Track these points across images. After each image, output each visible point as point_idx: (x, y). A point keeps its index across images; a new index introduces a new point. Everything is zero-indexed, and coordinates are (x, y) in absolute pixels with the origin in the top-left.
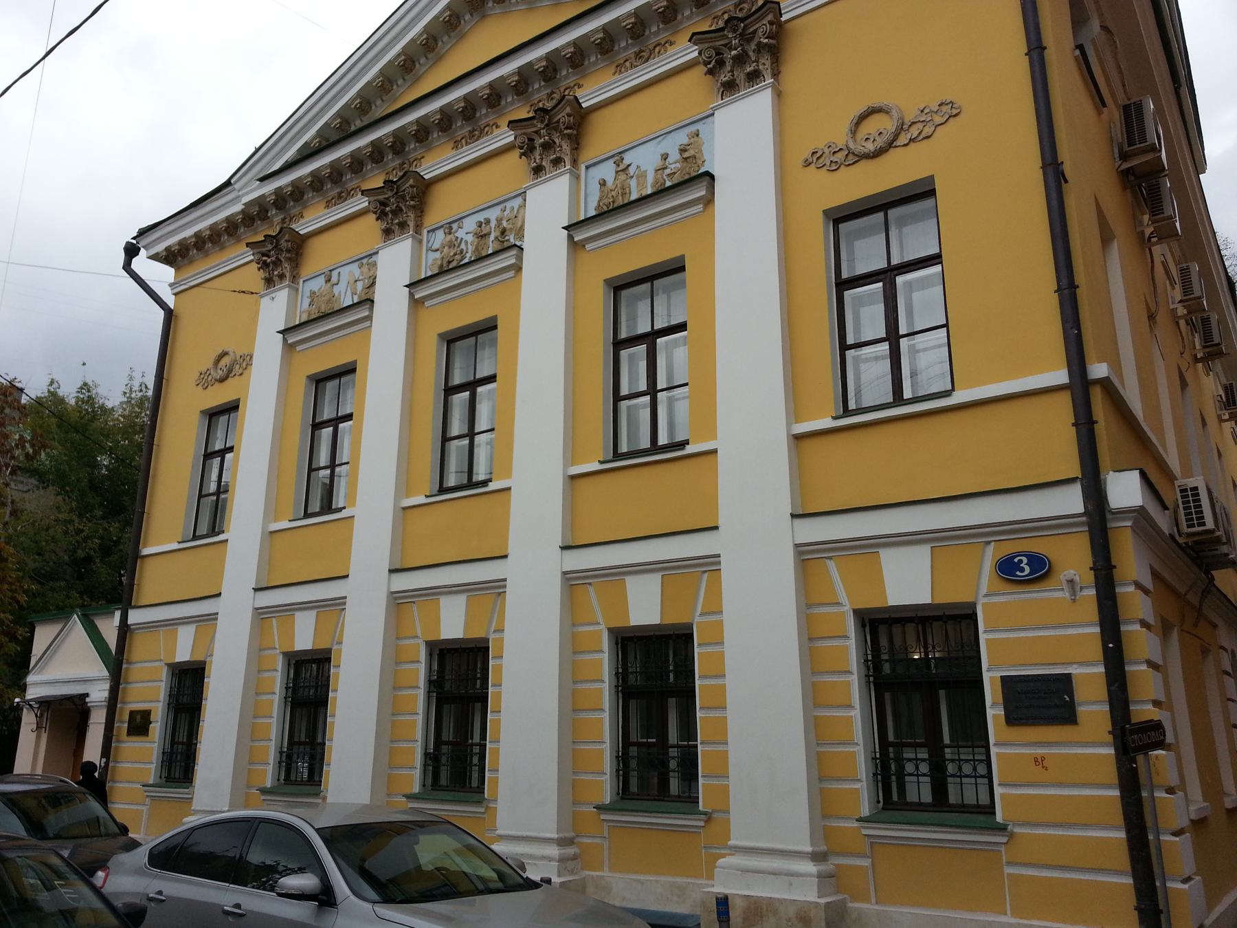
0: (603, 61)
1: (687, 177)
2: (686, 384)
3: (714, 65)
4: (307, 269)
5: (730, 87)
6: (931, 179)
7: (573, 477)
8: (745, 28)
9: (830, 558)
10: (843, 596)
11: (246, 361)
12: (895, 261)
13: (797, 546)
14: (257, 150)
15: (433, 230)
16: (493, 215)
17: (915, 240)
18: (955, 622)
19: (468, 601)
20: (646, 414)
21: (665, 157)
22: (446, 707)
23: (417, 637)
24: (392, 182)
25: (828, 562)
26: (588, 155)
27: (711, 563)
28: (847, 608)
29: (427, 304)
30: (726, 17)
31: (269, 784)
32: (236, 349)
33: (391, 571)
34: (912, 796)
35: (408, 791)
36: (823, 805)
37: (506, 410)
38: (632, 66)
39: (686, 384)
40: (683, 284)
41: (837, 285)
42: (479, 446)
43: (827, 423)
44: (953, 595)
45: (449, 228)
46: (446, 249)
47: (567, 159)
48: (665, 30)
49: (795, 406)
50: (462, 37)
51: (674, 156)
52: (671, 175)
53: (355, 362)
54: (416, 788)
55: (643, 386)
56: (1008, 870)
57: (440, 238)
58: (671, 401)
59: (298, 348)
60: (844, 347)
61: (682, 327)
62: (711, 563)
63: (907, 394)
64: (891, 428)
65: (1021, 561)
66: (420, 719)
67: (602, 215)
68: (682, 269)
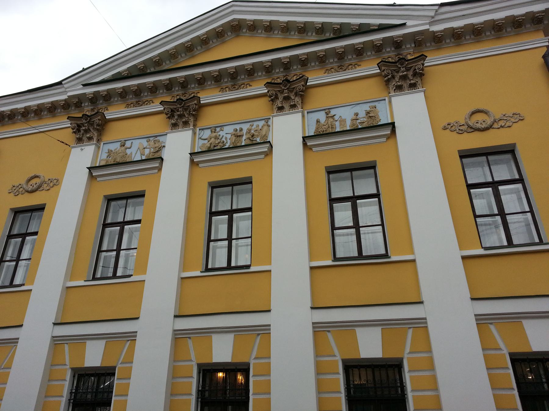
0: (120, 101)
1: (372, 125)
2: (136, 248)
3: (77, 129)
4: (202, 123)
5: (175, 126)
6: (514, 145)
7: (182, 278)
8: (407, 65)
9: (491, 324)
10: (336, 352)
11: (56, 183)
12: (234, 207)
13: (313, 323)
14: (84, 70)
15: (203, 129)
16: (245, 127)
17: (365, 186)
20: (113, 260)
21: (357, 114)
22: (76, 409)
23: (191, 360)
24: (182, 100)
25: (66, 345)
26: (105, 139)
27: (132, 336)
28: (505, 352)
29: (200, 165)
30: (178, 97)
32: (46, 175)
33: (176, 316)
37: (37, 251)
38: (134, 106)
39: (136, 248)
41: (210, 213)
42: (20, 266)
43: (198, 273)
44: (392, 354)
45: (213, 129)
46: (213, 140)
47: (95, 139)
48: (198, 88)
49: (184, 265)
50: (224, 42)
51: (362, 114)
52: (361, 123)
53: (45, 204)
57: (207, 134)
58: (237, 245)
59: (98, 179)
60: (209, 240)
61: (139, 222)
62: (132, 336)
67: (317, 136)
68: (143, 196)
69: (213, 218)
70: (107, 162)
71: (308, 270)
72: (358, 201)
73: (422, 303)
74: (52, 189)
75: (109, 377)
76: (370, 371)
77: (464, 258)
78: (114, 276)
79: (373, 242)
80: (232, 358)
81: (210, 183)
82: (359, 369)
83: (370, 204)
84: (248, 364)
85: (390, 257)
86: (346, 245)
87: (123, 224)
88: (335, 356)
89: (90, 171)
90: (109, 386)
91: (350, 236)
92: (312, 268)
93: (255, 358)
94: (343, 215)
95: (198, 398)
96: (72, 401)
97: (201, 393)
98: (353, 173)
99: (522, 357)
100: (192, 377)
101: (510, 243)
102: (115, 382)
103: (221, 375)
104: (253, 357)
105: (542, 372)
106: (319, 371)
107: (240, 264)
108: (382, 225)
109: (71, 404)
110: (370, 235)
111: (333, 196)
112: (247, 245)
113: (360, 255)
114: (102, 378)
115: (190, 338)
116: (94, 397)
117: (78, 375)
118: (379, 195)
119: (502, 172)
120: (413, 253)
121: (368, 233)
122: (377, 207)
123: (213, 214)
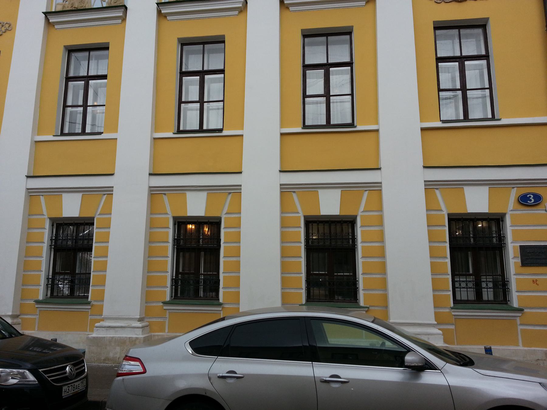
7: (155, 139)
9: (437, 189)
10: (299, 209)
12: (206, 68)
13: (281, 185)
17: (339, 53)
18: (496, 220)
19: (207, 195)
22: (58, 254)
23: (167, 214)
25: (41, 197)
28: (445, 213)
31: (41, 298)
34: (485, 298)
35: (163, 300)
36: (147, 296)
40: (107, 57)
41: (180, 73)
49: (156, 126)
54: (168, 299)
55: (80, 103)
56: (520, 327)
59: (56, 27)
60: (180, 102)
61: (104, 77)
62: (108, 191)
63: (88, 130)
64: (468, 131)
65: (530, 197)
66: (170, 260)
69: (184, 78)
70: (64, 7)
71: (279, 135)
72: (331, 69)
73: (380, 169)
74: (4, 34)
75: (88, 227)
76: (327, 227)
77: (423, 129)
78: (83, 132)
79: (341, 111)
80: (205, 213)
81: (179, 40)
82: (318, 224)
83: (342, 73)
84: (220, 219)
85: (355, 127)
86: (316, 112)
87: (88, 78)
88: (298, 213)
89: (46, 16)
90: (89, 234)
91: (319, 105)
92: (282, 134)
93: (226, 213)
94: (192, 87)
95: (174, 245)
96: (53, 247)
97: (177, 241)
98: (329, 38)
99: (458, 217)
100: (300, 227)
101: (466, 117)
102: (95, 231)
103: (190, 226)
104: (225, 212)
105: (471, 229)
106: (284, 224)
107: (211, 127)
108: (352, 95)
109: (53, 250)
110: (339, 104)
111: (307, 63)
112: (218, 109)
113: (328, 124)
114: (81, 228)
115: (165, 194)
116: (74, 244)
117: (57, 224)
118: (352, 63)
119: (339, 53)
120: (377, 123)
121: (337, 102)
122: (348, 77)
123: (183, 74)
